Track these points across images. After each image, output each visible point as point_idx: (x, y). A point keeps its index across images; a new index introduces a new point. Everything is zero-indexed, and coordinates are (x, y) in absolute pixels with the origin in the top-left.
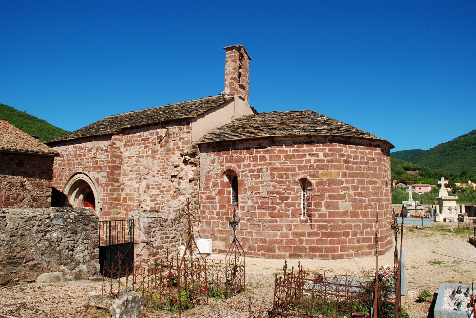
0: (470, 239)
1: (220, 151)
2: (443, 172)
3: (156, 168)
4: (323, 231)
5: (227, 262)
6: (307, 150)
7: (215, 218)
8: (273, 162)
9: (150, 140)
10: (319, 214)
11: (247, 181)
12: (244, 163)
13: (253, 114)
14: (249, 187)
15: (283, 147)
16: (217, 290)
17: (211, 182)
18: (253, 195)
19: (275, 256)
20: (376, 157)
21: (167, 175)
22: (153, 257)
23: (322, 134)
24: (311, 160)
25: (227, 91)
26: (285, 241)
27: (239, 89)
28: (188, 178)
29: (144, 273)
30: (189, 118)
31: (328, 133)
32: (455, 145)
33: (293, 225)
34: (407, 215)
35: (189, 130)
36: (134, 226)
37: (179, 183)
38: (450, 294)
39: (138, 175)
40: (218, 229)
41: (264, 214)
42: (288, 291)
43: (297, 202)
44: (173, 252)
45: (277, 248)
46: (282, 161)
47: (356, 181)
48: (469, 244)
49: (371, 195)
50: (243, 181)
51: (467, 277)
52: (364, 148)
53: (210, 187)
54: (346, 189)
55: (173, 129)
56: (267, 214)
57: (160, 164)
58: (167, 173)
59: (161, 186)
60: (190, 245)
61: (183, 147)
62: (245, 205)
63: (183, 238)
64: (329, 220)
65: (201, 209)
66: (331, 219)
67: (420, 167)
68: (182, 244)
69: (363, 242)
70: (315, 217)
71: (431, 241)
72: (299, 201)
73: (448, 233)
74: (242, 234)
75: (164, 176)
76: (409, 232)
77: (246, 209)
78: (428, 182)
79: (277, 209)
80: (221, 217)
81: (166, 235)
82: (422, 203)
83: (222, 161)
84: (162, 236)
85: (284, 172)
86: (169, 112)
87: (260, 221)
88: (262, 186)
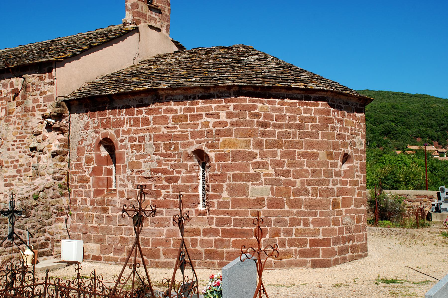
1: (93, 111)
3: (11, 137)
4: (225, 227)
6: (203, 108)
7: (88, 210)
9: (3, 94)
10: (219, 203)
11: (127, 154)
14: (130, 164)
15: (171, 105)
17: (84, 156)
18: (134, 175)
19: (158, 264)
20: (317, 116)
21: (26, 147)
24: (209, 122)
25: (129, 17)
26: (172, 242)
27: (149, 13)
35: (52, 80)
37: (39, 158)
40: (92, 225)
43: (192, 185)
45: (161, 252)
46: (170, 125)
47: (279, 154)
50: (121, 154)
52: (295, 103)
53: (83, 164)
58: (25, 144)
59: (18, 164)
62: (124, 189)
64: (232, 211)
70: (214, 207)
74: (121, 232)
75: (21, 148)
77: (126, 195)
79: (163, 195)
80: (95, 208)
83: (96, 125)
85: (172, 141)
88: (144, 162)
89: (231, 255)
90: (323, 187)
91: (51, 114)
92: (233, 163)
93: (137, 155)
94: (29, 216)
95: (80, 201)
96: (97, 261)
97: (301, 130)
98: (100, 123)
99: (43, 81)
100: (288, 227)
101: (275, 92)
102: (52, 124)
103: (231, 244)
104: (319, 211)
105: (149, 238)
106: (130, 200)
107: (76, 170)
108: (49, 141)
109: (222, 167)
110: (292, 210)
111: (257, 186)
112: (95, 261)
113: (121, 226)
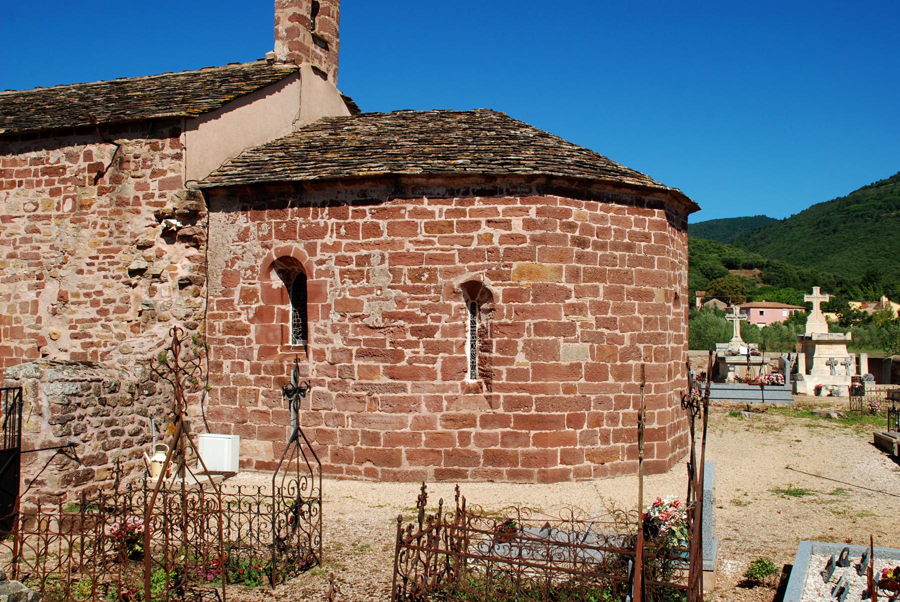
0: (876, 437)
1: (262, 208)
2: (820, 274)
3: (85, 250)
4: (520, 413)
5: (276, 492)
6: (482, 210)
7: (247, 382)
8: (397, 238)
9: (68, 172)
11: (331, 286)
12: (324, 241)
13: (348, 114)
14: (337, 302)
15: (422, 203)
16: (251, 564)
17: (239, 287)
18: (347, 321)
19: (399, 475)
20: (653, 232)
21: (119, 269)
22: (75, 486)
23: (520, 170)
24: (492, 236)
25: (280, 50)
26: (424, 438)
27: (312, 47)
28: (177, 278)
29: (47, 530)
30: (178, 119)
31: (535, 168)
32: (854, 206)
33: (446, 398)
34: (726, 377)
36: (21, 405)
37: (152, 291)
38: (822, 568)
39: (33, 269)
40: (255, 408)
41: (373, 371)
42: (429, 559)
43: (457, 341)
44: (132, 472)
45: (404, 455)
46: (421, 238)
47: (601, 291)
48: (875, 449)
49: (638, 326)
50: (320, 286)
51: (866, 529)
52: (624, 209)
53: (236, 302)
54: (577, 309)
55: (135, 147)
56: (382, 369)
57: (98, 238)
58: (118, 263)
59: (101, 298)
60: (178, 448)
61: (161, 196)
62: (324, 346)
63: (162, 433)
64: (533, 386)
65: (212, 359)
66: (539, 382)
67: (765, 261)
68: (159, 448)
69: (615, 442)
70: (500, 379)
71: (781, 441)
72: (460, 338)
73: (824, 423)
74: (318, 421)
76: (730, 419)
77: (329, 356)
78: (783, 296)
79: (406, 358)
80: (262, 378)
81: (114, 428)
82: (763, 348)
83: (265, 233)
84: (103, 428)
85: (424, 266)
86: (120, 98)
87: (362, 387)
89: (531, 458)
90: (660, 346)
91: (176, 211)
92: (535, 305)
93: (352, 289)
94: (154, 393)
95: (230, 366)
96: (268, 471)
97: (632, 254)
98: (273, 231)
99: (158, 152)
100: (612, 411)
101: (596, 190)
102: (175, 229)
103: (531, 440)
104: (653, 384)
105: (379, 431)
106: (337, 365)
107: (220, 312)
108: (169, 259)
109: (515, 312)
110: (619, 382)
111: (571, 344)
112: (264, 471)
113: (318, 410)
